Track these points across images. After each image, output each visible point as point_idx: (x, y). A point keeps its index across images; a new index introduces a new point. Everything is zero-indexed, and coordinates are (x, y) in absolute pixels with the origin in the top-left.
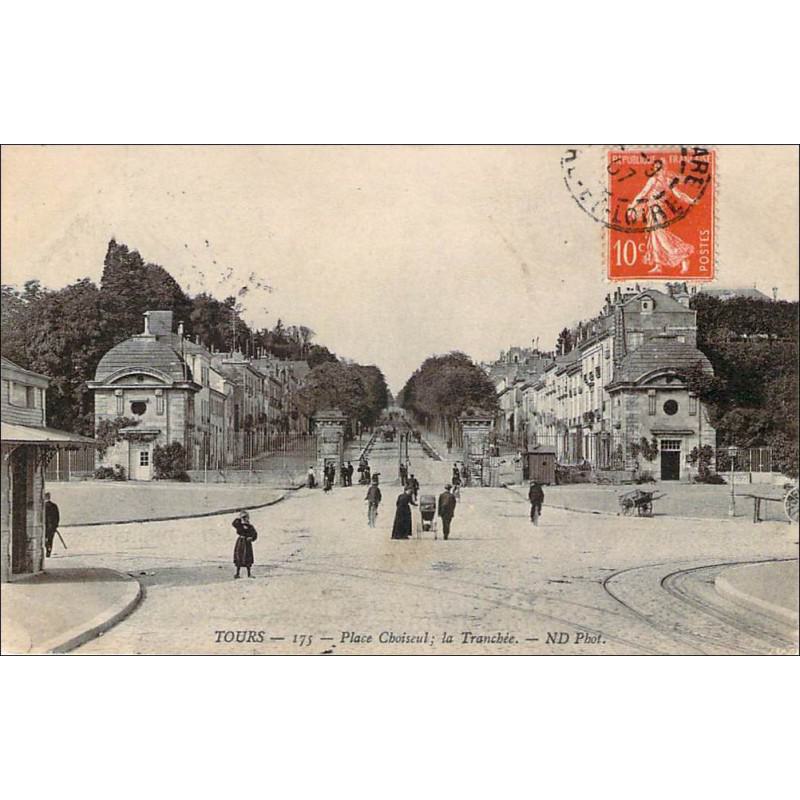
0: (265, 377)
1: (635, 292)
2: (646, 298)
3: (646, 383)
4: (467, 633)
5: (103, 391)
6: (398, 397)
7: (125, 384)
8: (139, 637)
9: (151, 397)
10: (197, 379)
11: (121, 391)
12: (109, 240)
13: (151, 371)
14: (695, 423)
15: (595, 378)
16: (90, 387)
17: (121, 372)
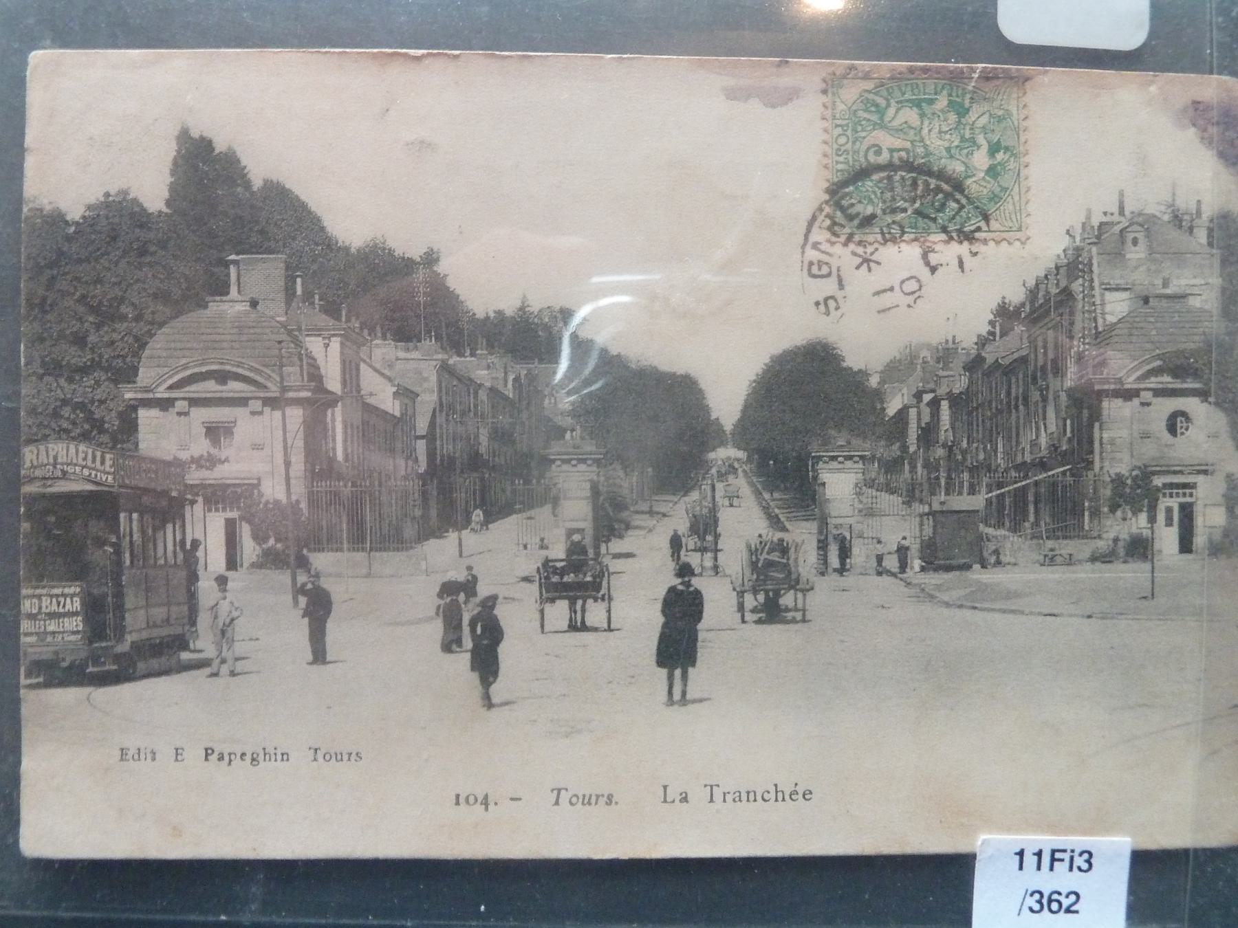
0: (480, 385)
1: (1116, 218)
2: (1135, 228)
3: (170, 388)
4: (559, 790)
5: (148, 403)
6: (733, 434)
7: (195, 390)
8: (459, 425)
9: (240, 413)
10: (334, 384)
11: (185, 403)
12: (635, 553)
13: (239, 365)
14: (71, 339)
15: (1050, 376)
16: (128, 396)
17: (185, 367)
